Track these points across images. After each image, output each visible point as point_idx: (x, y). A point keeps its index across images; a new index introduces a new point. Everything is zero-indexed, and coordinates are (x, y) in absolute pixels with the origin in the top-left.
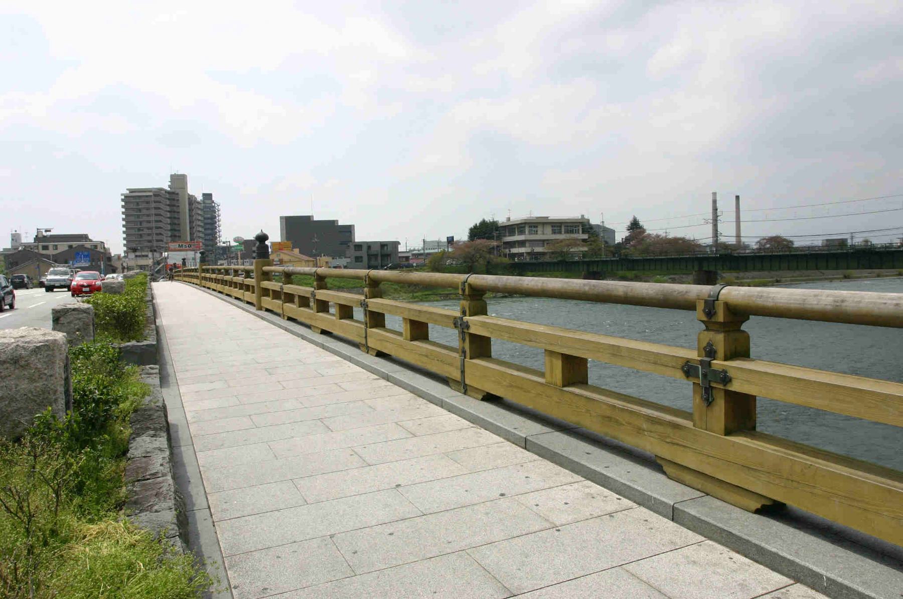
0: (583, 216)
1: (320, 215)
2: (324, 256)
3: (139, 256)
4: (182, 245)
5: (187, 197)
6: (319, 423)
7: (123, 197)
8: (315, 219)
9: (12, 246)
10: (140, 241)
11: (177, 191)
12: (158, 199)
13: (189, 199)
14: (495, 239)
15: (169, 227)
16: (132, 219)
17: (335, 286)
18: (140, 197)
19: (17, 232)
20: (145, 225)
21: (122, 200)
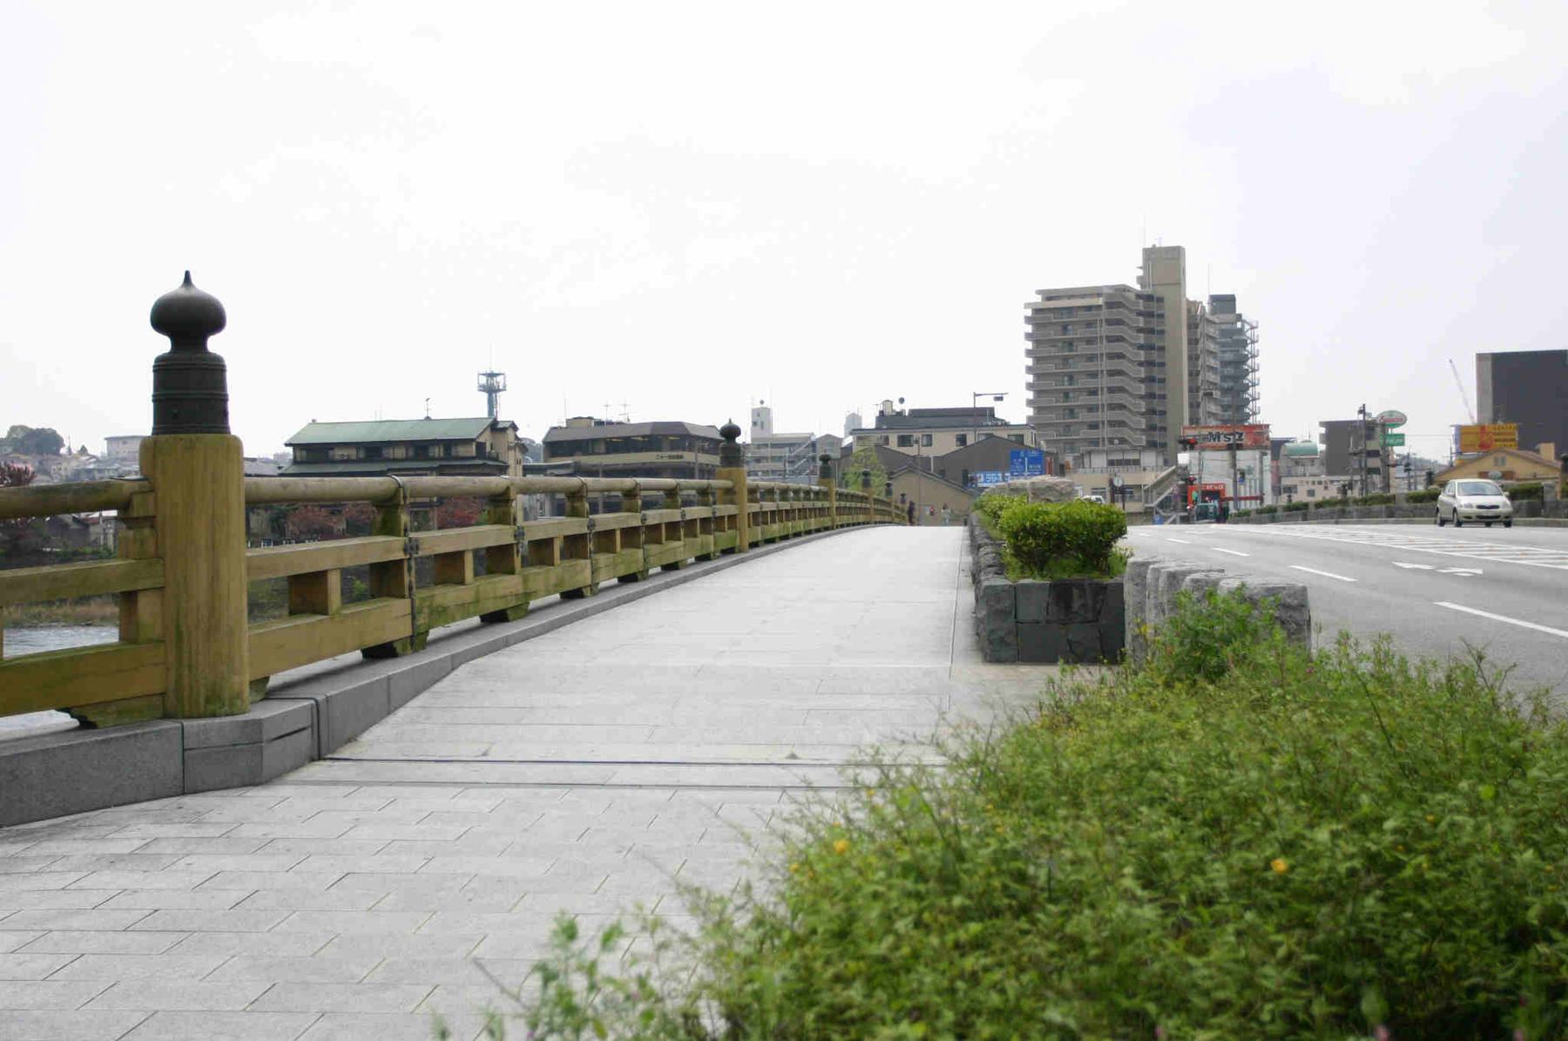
1: (34, 425)
3: (1119, 463)
5: (1184, 306)
7: (1029, 313)
9: (753, 439)
10: (1068, 426)
11: (1160, 292)
12: (1115, 314)
13: (1189, 311)
15: (1142, 389)
18: (1070, 310)
19: (764, 405)
21: (1028, 320)
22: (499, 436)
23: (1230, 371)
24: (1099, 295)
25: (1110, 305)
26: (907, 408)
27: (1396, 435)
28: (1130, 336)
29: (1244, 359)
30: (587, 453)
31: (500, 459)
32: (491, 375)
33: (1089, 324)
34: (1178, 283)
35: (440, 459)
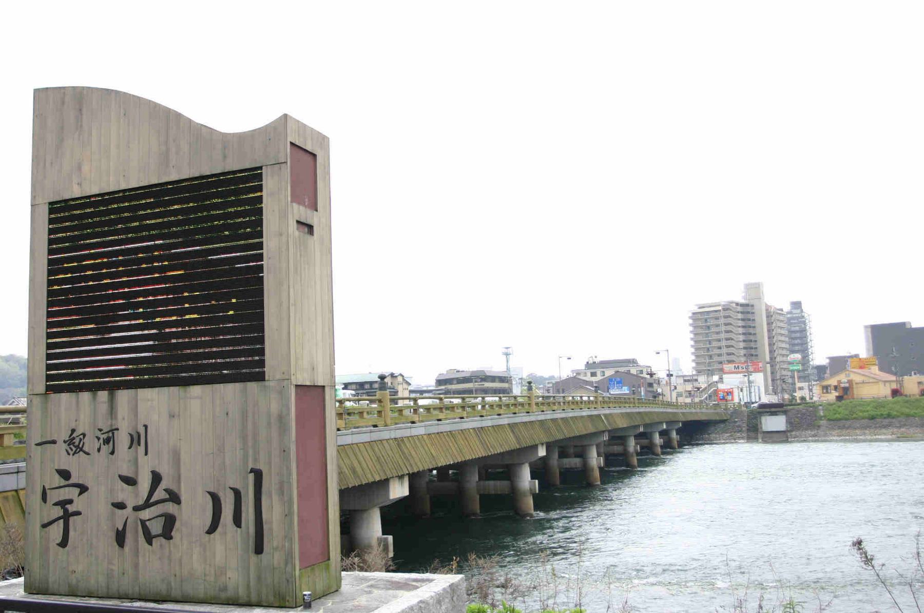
2: (915, 374)
4: (738, 366)
5: (764, 308)
6: (907, 588)
7: (690, 315)
8: (914, 326)
11: (752, 302)
12: (727, 313)
13: (767, 310)
14: (474, 392)
17: (902, 414)
18: (708, 312)
20: (715, 344)
21: (690, 318)
24: (719, 305)
25: (724, 310)
27: (579, 379)
28: (734, 323)
31: (395, 388)
35: (368, 389)
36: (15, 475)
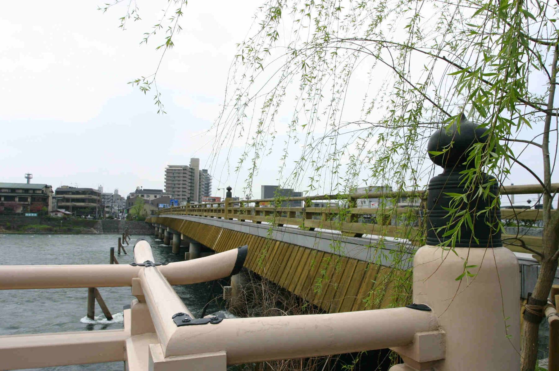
0: (116, 191)
7: (166, 170)
11: (194, 168)
16: (170, 182)
18: (175, 170)
22: (47, 188)
23: (206, 185)
24: (182, 167)
26: (143, 189)
29: (209, 183)
30: (66, 194)
32: (29, 175)
33: (179, 173)
34: (198, 166)
35: (32, 193)
36: (548, 6)
